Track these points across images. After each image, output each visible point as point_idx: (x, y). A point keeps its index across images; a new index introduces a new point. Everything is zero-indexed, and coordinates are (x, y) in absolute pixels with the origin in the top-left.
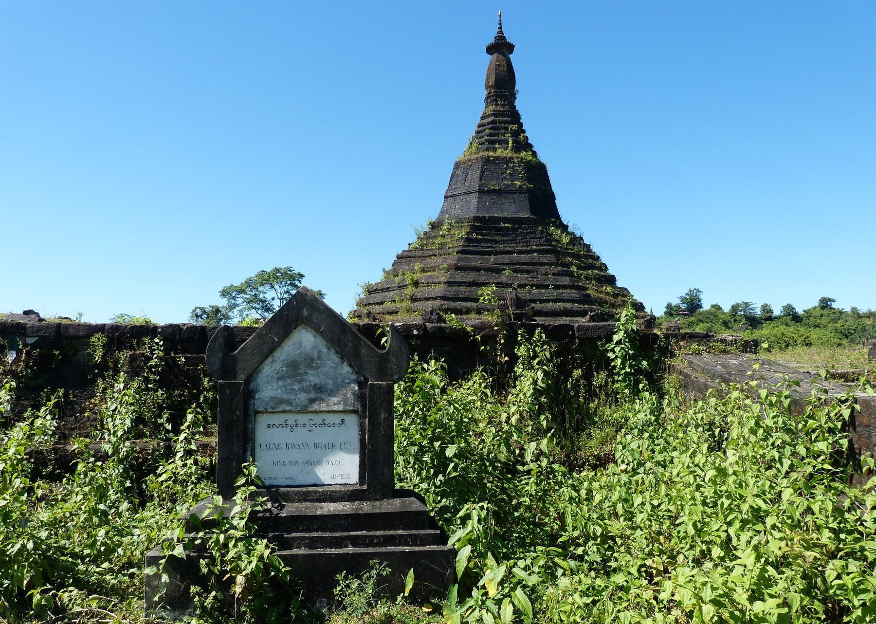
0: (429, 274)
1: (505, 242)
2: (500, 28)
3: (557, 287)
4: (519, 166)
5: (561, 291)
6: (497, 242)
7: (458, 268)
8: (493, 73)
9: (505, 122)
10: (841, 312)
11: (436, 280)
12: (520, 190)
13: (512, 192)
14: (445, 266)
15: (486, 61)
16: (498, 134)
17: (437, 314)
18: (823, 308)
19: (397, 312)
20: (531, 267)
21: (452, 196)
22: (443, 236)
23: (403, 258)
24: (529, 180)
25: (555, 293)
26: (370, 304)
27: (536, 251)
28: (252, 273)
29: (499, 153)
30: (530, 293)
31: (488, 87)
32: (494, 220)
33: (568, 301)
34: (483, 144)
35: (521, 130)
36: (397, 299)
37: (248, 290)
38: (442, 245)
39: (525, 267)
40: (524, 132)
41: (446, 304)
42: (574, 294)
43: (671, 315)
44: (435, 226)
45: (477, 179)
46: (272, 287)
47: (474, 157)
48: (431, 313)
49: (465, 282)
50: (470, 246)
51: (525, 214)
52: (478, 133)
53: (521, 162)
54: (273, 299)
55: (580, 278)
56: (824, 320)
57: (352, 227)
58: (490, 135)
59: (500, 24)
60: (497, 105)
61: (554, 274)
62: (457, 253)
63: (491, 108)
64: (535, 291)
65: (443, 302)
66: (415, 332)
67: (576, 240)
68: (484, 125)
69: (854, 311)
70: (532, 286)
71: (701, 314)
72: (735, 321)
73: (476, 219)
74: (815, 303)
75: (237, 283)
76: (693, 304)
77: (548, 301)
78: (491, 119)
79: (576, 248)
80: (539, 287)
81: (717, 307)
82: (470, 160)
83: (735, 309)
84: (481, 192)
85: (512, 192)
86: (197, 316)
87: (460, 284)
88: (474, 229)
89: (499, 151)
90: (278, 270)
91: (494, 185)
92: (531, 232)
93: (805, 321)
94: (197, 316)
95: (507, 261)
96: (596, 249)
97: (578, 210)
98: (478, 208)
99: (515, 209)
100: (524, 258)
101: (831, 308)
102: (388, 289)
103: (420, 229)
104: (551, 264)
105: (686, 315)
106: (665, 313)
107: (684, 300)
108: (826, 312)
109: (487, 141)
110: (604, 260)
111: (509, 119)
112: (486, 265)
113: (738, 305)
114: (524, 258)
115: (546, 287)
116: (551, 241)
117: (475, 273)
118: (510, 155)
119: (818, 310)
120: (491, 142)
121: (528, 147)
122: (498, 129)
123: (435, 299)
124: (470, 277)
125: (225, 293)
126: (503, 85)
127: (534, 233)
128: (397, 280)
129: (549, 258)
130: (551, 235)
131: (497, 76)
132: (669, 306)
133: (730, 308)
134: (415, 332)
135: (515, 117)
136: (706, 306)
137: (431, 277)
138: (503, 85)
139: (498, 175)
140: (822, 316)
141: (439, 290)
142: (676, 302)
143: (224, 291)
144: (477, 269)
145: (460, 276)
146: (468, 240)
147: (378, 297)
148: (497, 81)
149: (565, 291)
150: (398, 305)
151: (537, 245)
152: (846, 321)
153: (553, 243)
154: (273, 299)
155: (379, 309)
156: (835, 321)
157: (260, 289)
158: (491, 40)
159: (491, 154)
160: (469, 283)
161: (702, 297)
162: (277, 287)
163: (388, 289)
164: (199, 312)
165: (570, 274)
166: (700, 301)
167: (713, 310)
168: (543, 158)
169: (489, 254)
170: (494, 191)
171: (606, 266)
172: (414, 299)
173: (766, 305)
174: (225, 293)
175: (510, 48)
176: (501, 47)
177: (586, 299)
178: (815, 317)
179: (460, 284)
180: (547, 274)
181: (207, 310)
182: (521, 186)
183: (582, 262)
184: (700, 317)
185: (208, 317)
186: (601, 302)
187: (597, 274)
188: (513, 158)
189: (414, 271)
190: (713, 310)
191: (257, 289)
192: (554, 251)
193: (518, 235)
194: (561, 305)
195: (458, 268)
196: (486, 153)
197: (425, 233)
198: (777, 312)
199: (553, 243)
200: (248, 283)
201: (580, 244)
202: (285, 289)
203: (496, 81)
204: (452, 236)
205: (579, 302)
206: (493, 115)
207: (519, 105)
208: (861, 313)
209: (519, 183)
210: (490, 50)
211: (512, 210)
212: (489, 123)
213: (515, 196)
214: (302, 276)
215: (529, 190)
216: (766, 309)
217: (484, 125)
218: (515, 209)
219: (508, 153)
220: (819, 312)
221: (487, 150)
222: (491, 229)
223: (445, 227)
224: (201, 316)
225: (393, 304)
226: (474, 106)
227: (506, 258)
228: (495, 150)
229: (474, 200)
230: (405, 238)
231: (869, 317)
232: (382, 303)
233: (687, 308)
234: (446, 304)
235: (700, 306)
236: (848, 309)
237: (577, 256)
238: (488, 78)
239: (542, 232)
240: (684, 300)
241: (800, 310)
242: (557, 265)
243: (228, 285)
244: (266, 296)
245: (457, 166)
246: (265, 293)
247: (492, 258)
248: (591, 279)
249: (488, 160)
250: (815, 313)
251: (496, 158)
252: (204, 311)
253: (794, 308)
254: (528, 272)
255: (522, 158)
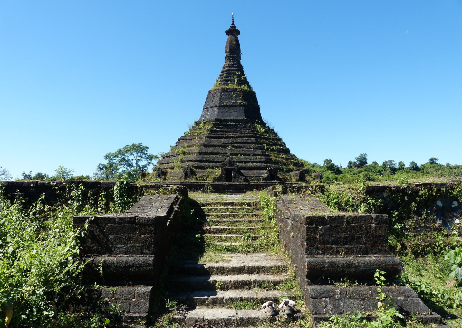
0: (191, 148)
1: (230, 132)
2: (233, 22)
3: (254, 155)
4: (240, 93)
5: (256, 157)
6: (226, 132)
7: (205, 145)
8: (229, 45)
9: (234, 70)
10: (441, 166)
11: (193, 152)
12: (240, 105)
13: (236, 106)
14: (198, 144)
15: (226, 38)
16: (230, 77)
17: (191, 169)
18: (431, 163)
19: (174, 168)
20: (242, 145)
21: (207, 108)
22: (200, 129)
23: (181, 140)
24: (245, 100)
25: (252, 158)
26: (162, 164)
27: (245, 136)
28: (122, 147)
29: (230, 86)
30: (240, 158)
31: (226, 52)
32: (228, 121)
33: (259, 162)
34: (222, 81)
35: (243, 73)
36: (175, 161)
37: (119, 155)
38: (200, 134)
39: (239, 145)
40: (244, 75)
41: (197, 164)
42: (262, 158)
43: (351, 167)
44: (197, 123)
45: (218, 100)
46: (132, 154)
47: (217, 88)
48: (187, 168)
49: (207, 153)
50: (212, 134)
51: (242, 118)
52: (221, 76)
53: (241, 91)
54: (132, 160)
55: (268, 150)
56: (432, 170)
57: (160, 122)
58: (226, 77)
59: (233, 20)
60: (230, 61)
61: (254, 148)
62: (206, 137)
63: (227, 63)
64: (243, 157)
65: (195, 163)
66: (32, 185)
67: (269, 131)
68: (224, 72)
69: (448, 165)
70: (241, 155)
71: (366, 167)
72: (385, 170)
73: (217, 120)
74: (428, 161)
75: (113, 152)
76: (362, 161)
77: (248, 162)
78: (227, 69)
79: (268, 135)
80: (245, 155)
81: (376, 163)
82: (215, 90)
83: (385, 164)
84: (220, 106)
85: (236, 106)
86: (101, 169)
87: (205, 153)
88: (215, 125)
89: (230, 85)
90: (134, 145)
91: (226, 103)
92: (244, 127)
93: (422, 170)
94: (101, 169)
95: (230, 142)
96: (280, 135)
97: (272, 114)
98: (218, 115)
99: (237, 115)
100: (239, 140)
101: (436, 164)
102: (171, 156)
103: (191, 125)
104: (252, 143)
105: (359, 167)
106: (348, 166)
107: (358, 159)
108: (433, 165)
109: (224, 80)
110: (284, 141)
111: (236, 69)
112: (219, 144)
113: (386, 162)
114: (239, 140)
115: (249, 155)
116: (254, 131)
117: (213, 148)
118: (235, 87)
119: (429, 164)
120: (227, 81)
121: (246, 82)
122: (230, 74)
123: (192, 161)
124: (210, 150)
125: (107, 157)
126: (234, 51)
127: (246, 127)
128: (176, 151)
129: (252, 140)
130: (255, 128)
131: (230, 46)
132: (350, 163)
133: (382, 164)
134: (32, 185)
135: (240, 68)
136: (370, 162)
137: (191, 150)
138: (234, 51)
139: (229, 97)
140: (431, 168)
141: (194, 156)
142: (353, 160)
143: (106, 156)
144: (214, 146)
145: (205, 150)
146: (211, 131)
147: (167, 160)
148: (230, 49)
149: (258, 157)
150: (175, 164)
151: (246, 134)
152: (444, 170)
153: (255, 132)
154: (132, 160)
155: (166, 166)
156: (437, 170)
157: (126, 154)
158: (228, 28)
159: (226, 86)
160: (209, 153)
161: (367, 158)
162: (134, 154)
163: (171, 156)
164: (101, 166)
165: (263, 148)
166: (366, 160)
167: (374, 164)
168: (254, 89)
169: (222, 138)
170: (226, 106)
171: (284, 144)
172: (182, 161)
173: (401, 162)
174: (107, 157)
175: (238, 32)
176: (233, 32)
177: (269, 161)
178: (427, 168)
179: (205, 153)
180: (250, 148)
181: (106, 165)
182: (240, 103)
183: (271, 142)
184: (366, 168)
185: (106, 169)
186: (277, 163)
187: (278, 148)
188: (237, 89)
189: (185, 147)
190: (374, 164)
191: (124, 155)
192: (255, 137)
193: (237, 128)
194: (255, 164)
195: (205, 145)
196: (223, 86)
197: (193, 127)
198: (407, 165)
199: (255, 132)
200: (119, 152)
201: (271, 132)
202: (139, 155)
203: (230, 49)
204: (204, 129)
205: (265, 163)
206: (228, 66)
207: (242, 62)
208: (451, 166)
209: (239, 102)
210: (228, 33)
211: (236, 115)
212: (226, 71)
213: (238, 108)
214: (148, 148)
215: (244, 105)
216: (401, 164)
217: (224, 72)
218: (237, 115)
219: (235, 86)
220: (429, 165)
221: (224, 84)
222: (224, 125)
223: (202, 124)
224: (102, 168)
225: (173, 164)
226: (219, 62)
227: (230, 140)
228: (228, 84)
229: (216, 110)
230: (183, 130)
231: (455, 168)
232: (168, 163)
233: (360, 163)
234: (197, 164)
235: (366, 163)
236: (444, 164)
237: (268, 139)
238: (226, 47)
239: (250, 126)
240: (358, 159)
241: (419, 165)
242: (256, 143)
243: (109, 153)
244: (129, 158)
245: (210, 92)
246: (128, 157)
247: (223, 140)
248: (274, 151)
249: (224, 90)
250: (427, 166)
251: (228, 89)
252: (104, 166)
253: (416, 164)
254: (240, 147)
255: (241, 89)
